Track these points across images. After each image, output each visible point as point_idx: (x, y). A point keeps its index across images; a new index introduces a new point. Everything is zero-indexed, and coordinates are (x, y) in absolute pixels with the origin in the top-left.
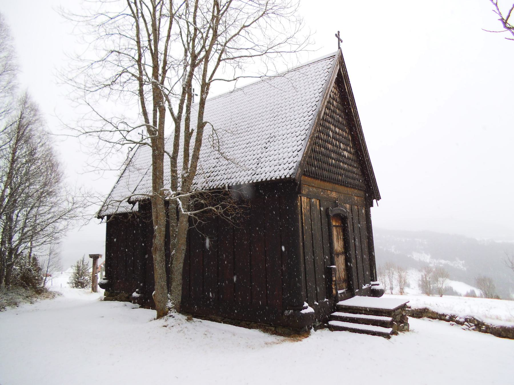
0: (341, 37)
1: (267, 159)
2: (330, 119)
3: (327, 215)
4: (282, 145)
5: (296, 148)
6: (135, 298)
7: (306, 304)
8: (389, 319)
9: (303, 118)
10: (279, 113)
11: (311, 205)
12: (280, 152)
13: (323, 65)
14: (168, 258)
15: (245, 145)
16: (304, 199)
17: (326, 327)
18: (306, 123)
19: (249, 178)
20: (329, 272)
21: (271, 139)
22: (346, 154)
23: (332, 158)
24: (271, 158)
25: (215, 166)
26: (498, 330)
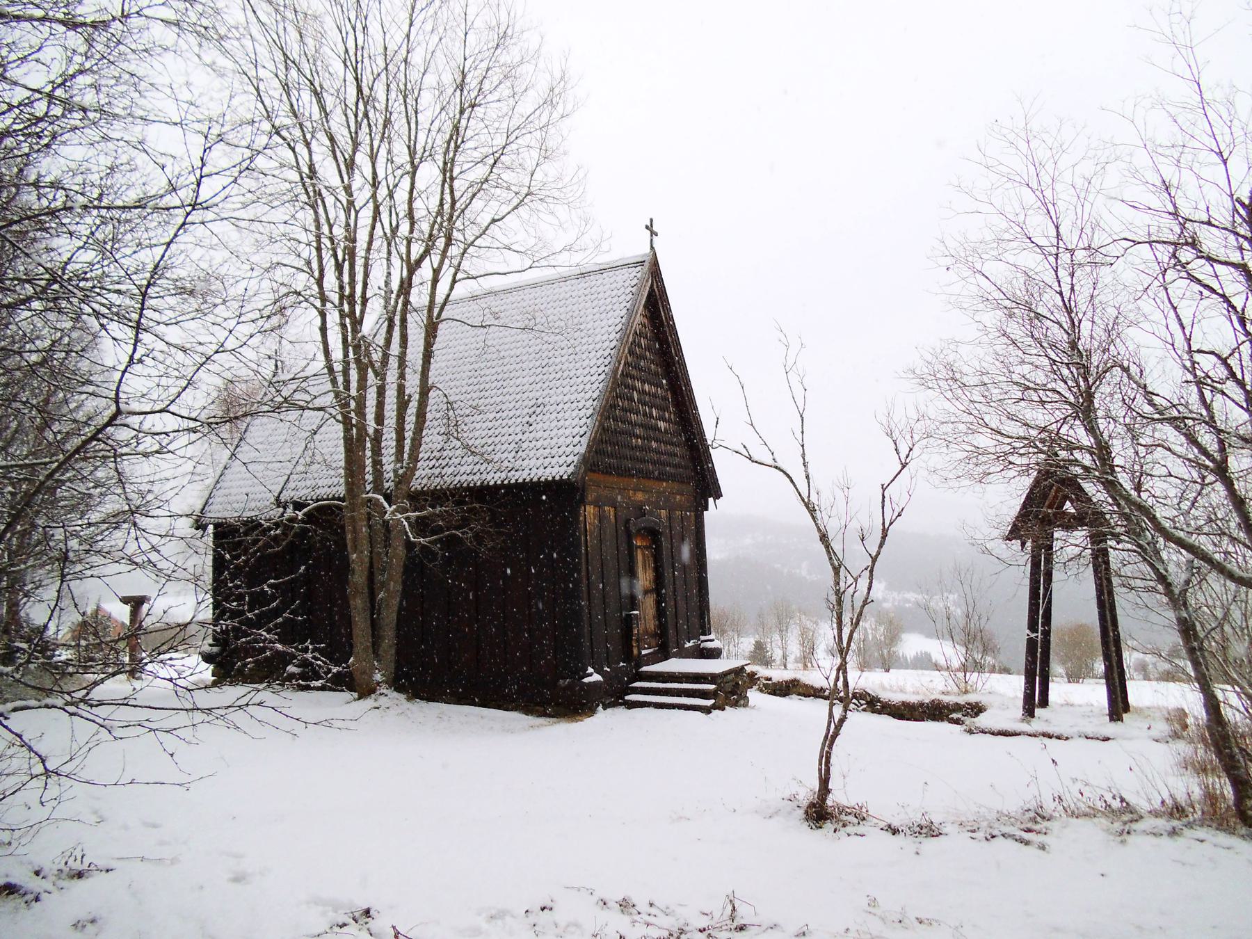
0: (655, 229)
1: (532, 445)
2: (634, 372)
3: (628, 530)
4: (555, 423)
5: (577, 429)
6: (292, 676)
7: (590, 670)
8: (712, 687)
9: (588, 377)
10: (551, 361)
11: (601, 518)
12: (553, 434)
13: (624, 278)
14: (373, 605)
15: (494, 414)
16: (590, 510)
17: (621, 704)
18: (596, 385)
19: (503, 475)
20: (628, 623)
21: (538, 407)
22: (661, 425)
23: (637, 437)
24: (539, 444)
25: (442, 449)
26: (899, 708)
